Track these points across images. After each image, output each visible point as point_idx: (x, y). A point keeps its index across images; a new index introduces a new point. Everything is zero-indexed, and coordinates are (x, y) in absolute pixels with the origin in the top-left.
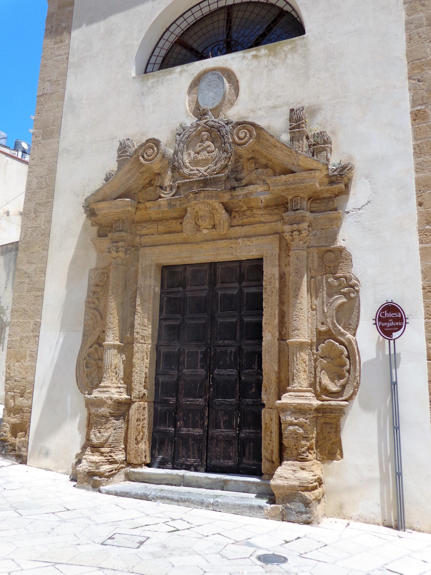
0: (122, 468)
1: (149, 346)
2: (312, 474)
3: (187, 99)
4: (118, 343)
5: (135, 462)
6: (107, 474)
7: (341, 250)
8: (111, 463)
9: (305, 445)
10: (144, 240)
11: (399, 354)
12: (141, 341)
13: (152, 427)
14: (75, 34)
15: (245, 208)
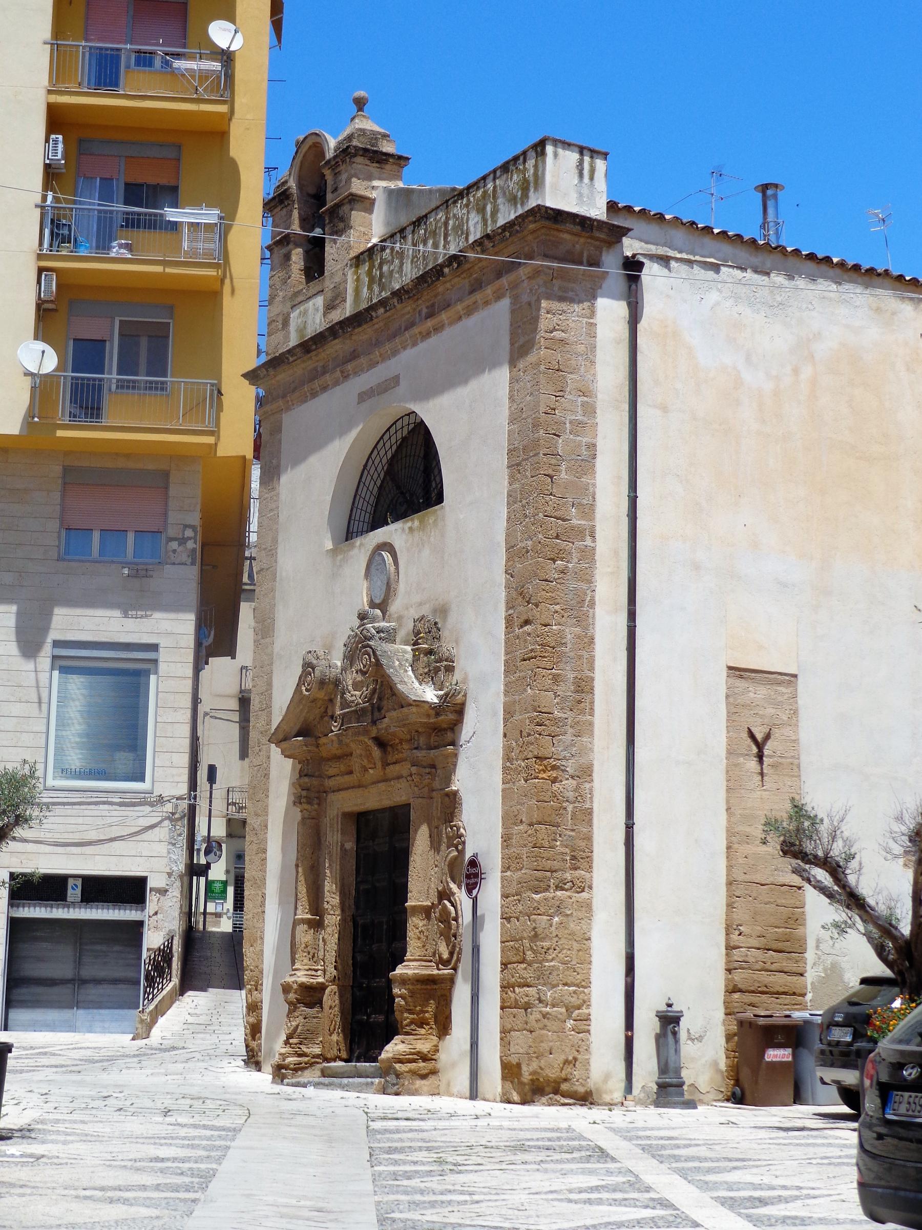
0: (318, 1063)
1: (339, 918)
2: (411, 1047)
3: (365, 586)
4: (309, 916)
5: (329, 1056)
6: (292, 1066)
7: (455, 794)
8: (300, 1055)
9: (408, 1018)
10: (331, 783)
11: (483, 916)
12: (332, 912)
13: (349, 1017)
14: (284, 479)
15: (397, 741)
